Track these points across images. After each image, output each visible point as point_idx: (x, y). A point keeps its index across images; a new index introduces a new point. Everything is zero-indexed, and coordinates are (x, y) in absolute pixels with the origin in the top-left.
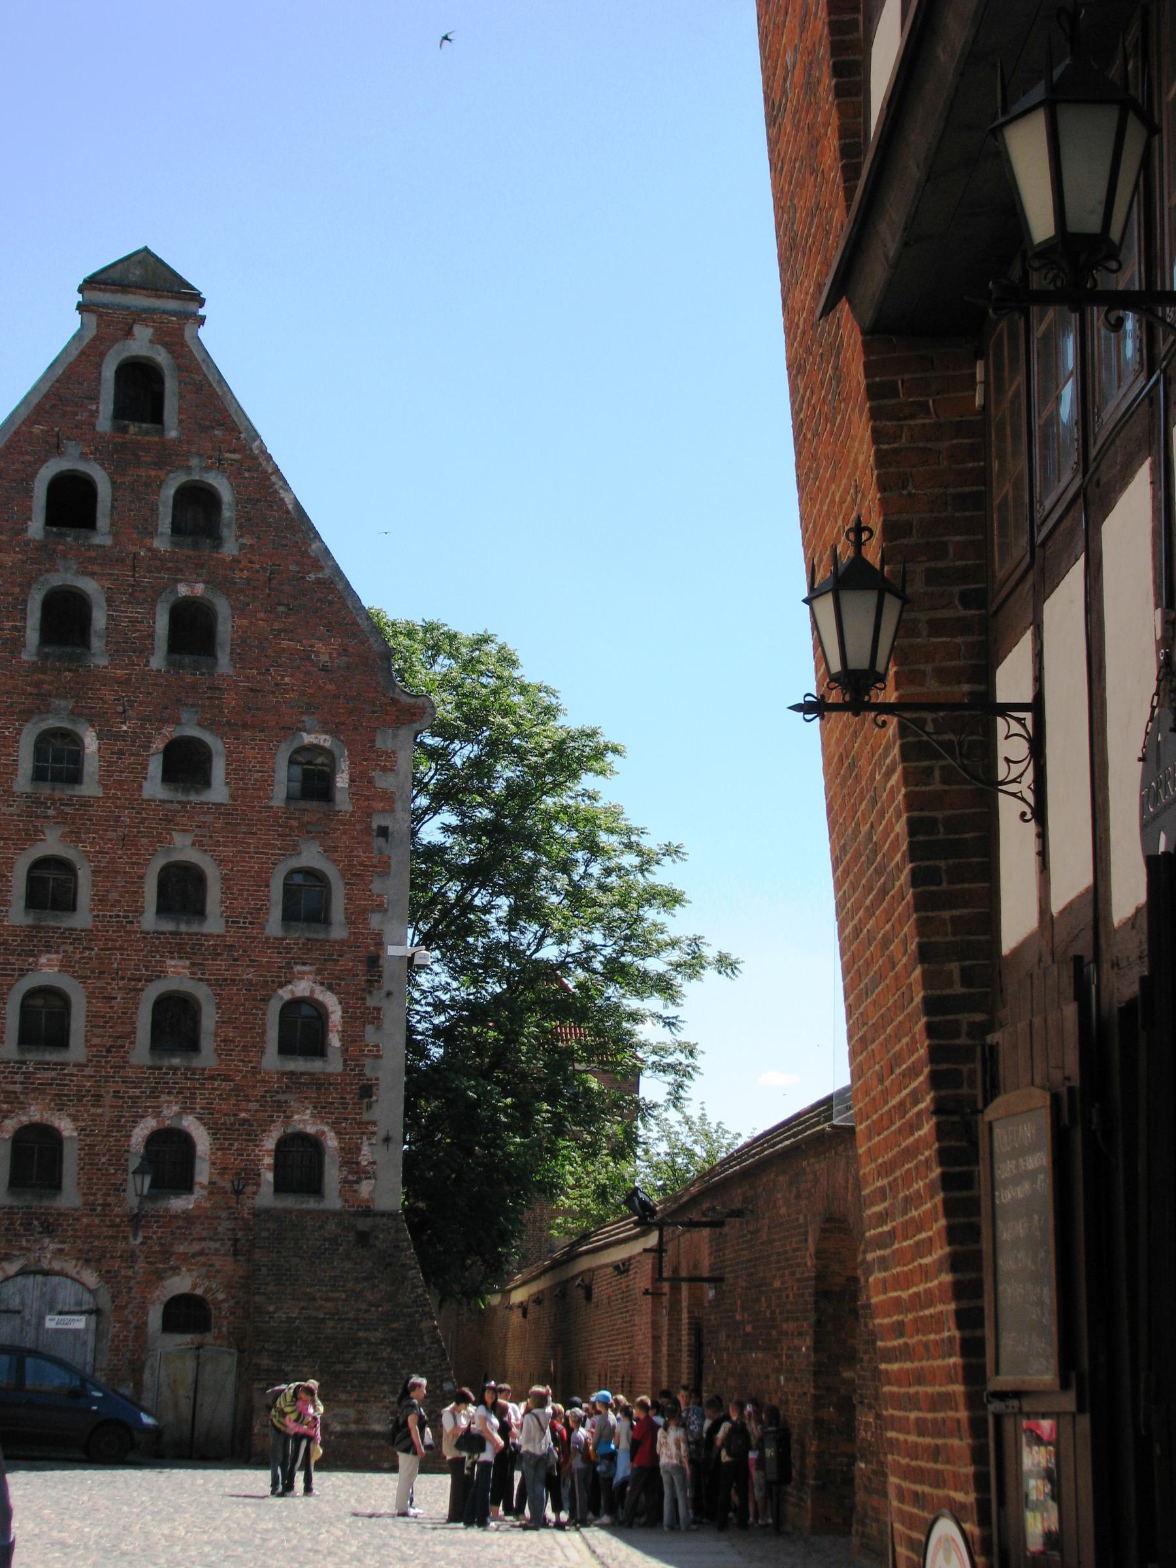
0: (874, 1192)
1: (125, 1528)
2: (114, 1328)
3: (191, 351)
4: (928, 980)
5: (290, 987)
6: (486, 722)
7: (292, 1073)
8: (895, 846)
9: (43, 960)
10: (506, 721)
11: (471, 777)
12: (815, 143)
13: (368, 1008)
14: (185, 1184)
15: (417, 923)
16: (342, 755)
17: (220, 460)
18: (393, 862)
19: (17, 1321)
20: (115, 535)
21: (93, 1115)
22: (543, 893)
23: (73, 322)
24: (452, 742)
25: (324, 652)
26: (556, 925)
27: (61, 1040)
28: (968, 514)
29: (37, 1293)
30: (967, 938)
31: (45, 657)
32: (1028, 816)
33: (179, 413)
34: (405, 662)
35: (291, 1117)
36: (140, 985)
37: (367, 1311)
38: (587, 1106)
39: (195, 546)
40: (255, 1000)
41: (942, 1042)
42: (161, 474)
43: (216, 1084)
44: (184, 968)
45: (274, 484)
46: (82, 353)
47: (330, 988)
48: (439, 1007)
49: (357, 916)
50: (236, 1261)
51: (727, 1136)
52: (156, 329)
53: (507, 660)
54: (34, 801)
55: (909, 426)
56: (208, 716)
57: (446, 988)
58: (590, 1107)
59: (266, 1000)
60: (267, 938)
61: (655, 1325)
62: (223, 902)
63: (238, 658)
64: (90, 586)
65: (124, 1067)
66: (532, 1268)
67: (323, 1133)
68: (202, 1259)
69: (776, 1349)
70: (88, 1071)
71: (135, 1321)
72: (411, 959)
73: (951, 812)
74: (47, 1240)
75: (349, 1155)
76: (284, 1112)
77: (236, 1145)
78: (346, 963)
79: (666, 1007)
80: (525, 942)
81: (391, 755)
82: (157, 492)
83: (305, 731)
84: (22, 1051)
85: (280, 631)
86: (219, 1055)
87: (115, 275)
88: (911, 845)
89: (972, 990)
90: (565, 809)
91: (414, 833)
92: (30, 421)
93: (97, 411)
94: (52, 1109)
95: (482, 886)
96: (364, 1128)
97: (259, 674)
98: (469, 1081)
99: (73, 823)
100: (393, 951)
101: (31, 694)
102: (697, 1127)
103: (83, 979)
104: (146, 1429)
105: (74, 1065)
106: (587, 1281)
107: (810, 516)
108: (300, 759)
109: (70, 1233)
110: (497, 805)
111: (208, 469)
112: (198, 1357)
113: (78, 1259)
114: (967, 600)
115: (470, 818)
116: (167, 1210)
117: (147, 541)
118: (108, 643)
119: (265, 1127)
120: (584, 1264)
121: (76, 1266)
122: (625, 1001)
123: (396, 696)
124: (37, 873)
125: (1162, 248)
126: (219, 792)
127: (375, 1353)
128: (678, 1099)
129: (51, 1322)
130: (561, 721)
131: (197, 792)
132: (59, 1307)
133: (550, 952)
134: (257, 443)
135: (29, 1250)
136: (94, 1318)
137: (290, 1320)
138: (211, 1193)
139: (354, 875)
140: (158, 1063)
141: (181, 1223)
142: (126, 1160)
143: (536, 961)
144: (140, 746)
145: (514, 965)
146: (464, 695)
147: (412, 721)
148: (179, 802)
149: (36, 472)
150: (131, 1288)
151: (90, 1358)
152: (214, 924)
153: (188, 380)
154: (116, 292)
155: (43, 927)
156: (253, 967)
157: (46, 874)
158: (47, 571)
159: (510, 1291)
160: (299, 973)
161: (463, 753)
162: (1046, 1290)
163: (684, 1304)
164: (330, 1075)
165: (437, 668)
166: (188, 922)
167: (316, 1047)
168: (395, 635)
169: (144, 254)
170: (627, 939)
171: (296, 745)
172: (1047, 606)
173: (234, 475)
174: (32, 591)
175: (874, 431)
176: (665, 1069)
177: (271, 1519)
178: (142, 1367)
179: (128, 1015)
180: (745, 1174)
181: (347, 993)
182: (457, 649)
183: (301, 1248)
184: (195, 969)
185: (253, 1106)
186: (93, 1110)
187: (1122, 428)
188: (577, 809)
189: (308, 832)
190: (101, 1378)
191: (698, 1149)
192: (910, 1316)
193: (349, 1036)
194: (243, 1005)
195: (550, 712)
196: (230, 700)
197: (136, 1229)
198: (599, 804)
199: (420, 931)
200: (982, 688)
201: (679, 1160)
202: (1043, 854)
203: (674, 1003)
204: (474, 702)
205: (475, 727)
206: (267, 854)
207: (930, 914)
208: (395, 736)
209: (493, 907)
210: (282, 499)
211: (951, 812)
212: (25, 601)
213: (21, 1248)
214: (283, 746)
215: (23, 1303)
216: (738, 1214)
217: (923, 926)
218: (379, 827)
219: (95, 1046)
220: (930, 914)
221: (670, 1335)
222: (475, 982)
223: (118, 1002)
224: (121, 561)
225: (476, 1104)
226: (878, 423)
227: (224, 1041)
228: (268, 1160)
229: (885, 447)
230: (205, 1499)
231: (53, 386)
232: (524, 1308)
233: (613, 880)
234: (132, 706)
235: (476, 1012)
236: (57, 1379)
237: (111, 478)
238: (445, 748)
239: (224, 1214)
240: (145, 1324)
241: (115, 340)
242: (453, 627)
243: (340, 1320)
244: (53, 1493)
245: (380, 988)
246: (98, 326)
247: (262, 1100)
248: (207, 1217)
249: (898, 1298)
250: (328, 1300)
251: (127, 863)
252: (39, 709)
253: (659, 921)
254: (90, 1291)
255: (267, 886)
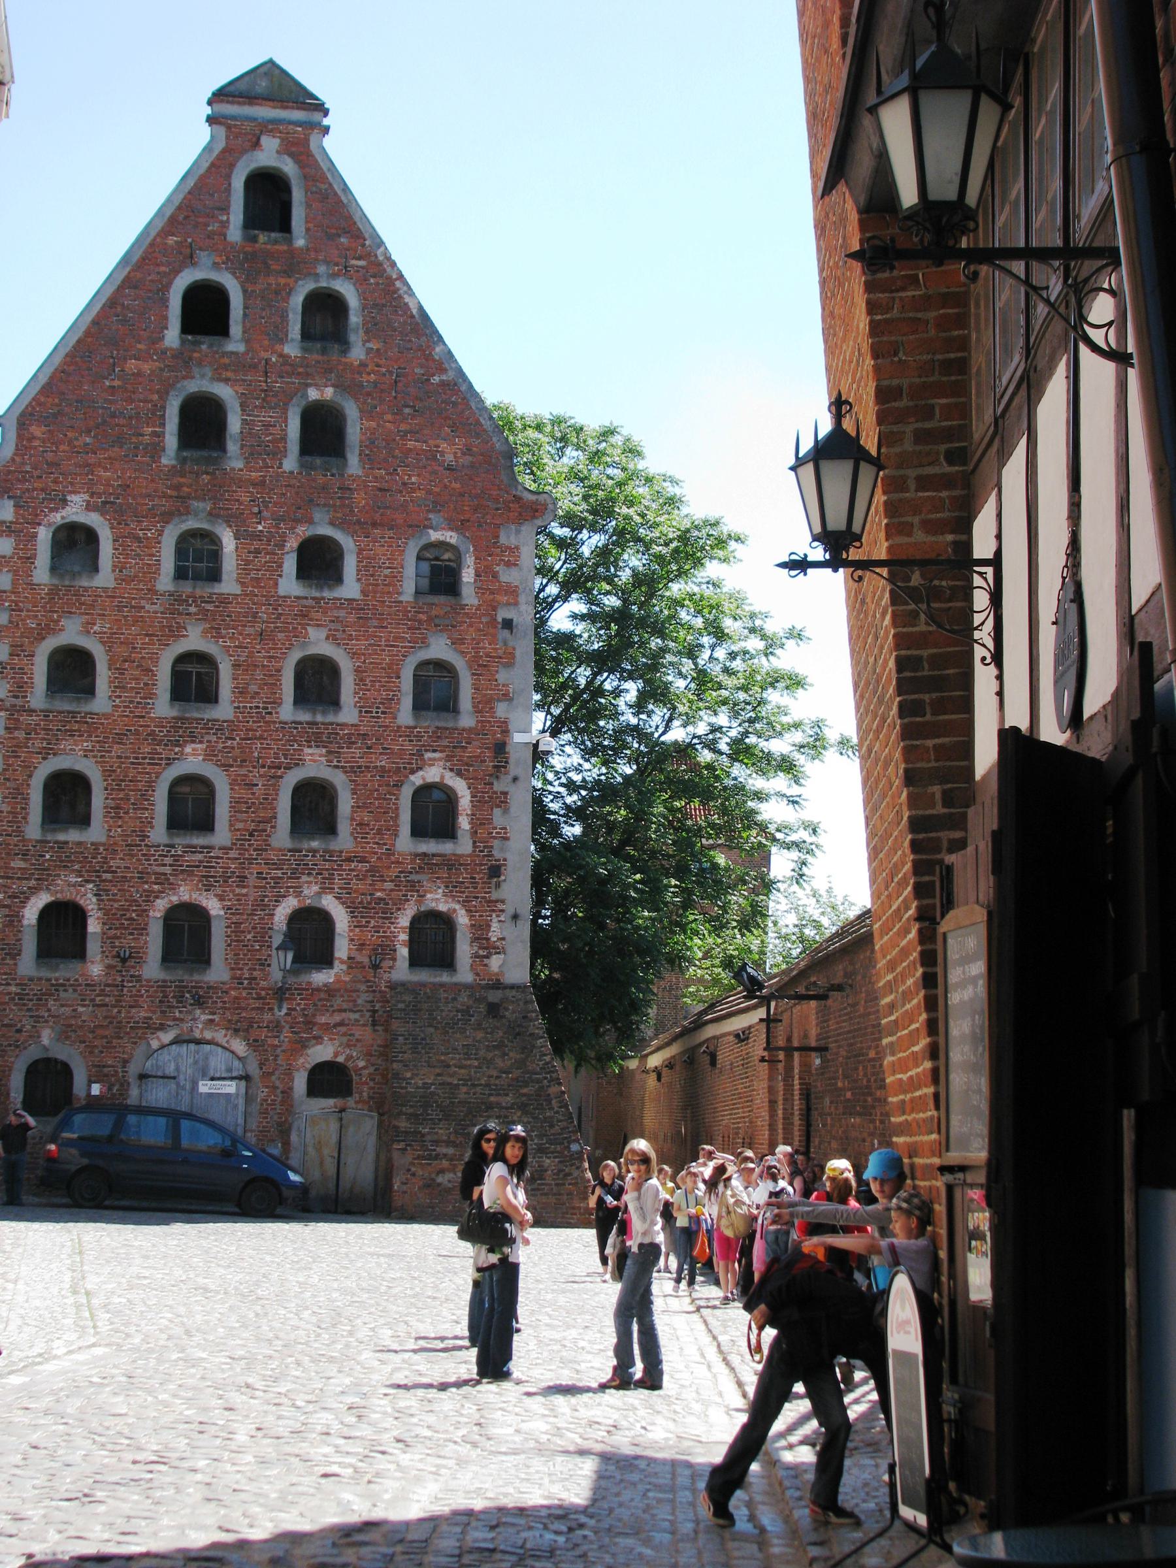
0: (885, 985)
1: (264, 1276)
2: (262, 1093)
3: (317, 161)
4: (913, 801)
5: (421, 773)
6: (610, 514)
7: (425, 854)
8: (889, 680)
9: (188, 749)
10: (631, 511)
11: (597, 565)
12: (827, 24)
13: (496, 793)
14: (325, 959)
15: (549, 708)
16: (468, 551)
17: (346, 267)
18: (518, 653)
19: (172, 1085)
20: (247, 341)
21: (238, 895)
22: (670, 678)
23: (204, 134)
24: (580, 533)
25: (449, 452)
26: (681, 709)
27: (206, 824)
28: (953, 378)
29: (191, 1061)
30: (948, 764)
31: (183, 461)
32: (988, 660)
33: (307, 222)
34: (533, 455)
35: (424, 896)
36: (279, 773)
37: (498, 1077)
38: (713, 881)
39: (324, 351)
40: (388, 785)
41: (924, 857)
42: (291, 281)
43: (353, 865)
44: (321, 756)
45: (398, 289)
46: (213, 165)
47: (459, 774)
48: (571, 787)
49: (484, 705)
50: (375, 1031)
51: (853, 908)
52: (282, 140)
53: (633, 451)
54: (177, 599)
55: (901, 298)
56: (339, 515)
57: (578, 769)
58: (718, 882)
59: (398, 785)
60: (399, 727)
61: (771, 1090)
62: (356, 693)
63: (367, 458)
64: (225, 392)
65: (266, 850)
66: (667, 1035)
67: (455, 910)
68: (343, 1029)
69: (871, 1115)
70: (233, 854)
71: (281, 1086)
72: (536, 746)
73: (935, 651)
74: (198, 1012)
75: (480, 933)
76: (418, 891)
77: (373, 923)
78: (473, 750)
79: (790, 786)
80: (653, 724)
81: (514, 550)
82: (286, 300)
83: (431, 528)
84: (170, 835)
85: (406, 432)
86: (356, 838)
87: (242, 86)
88: (900, 681)
89: (952, 810)
90: (691, 596)
91: (543, 622)
92: (165, 232)
93: (228, 221)
94: (200, 890)
95: (611, 671)
96: (493, 905)
97: (387, 474)
98: (599, 857)
99: (214, 620)
100: (518, 738)
101: (171, 497)
102: (824, 899)
103: (226, 767)
104: (293, 1185)
105: (220, 849)
106: (712, 1048)
107: (831, 366)
108: (428, 555)
109: (220, 1005)
110: (624, 594)
111: (334, 276)
112: (341, 1119)
113: (227, 1029)
114: (951, 457)
115: (598, 605)
116: (309, 983)
117: (278, 347)
118: (242, 448)
119: (400, 904)
120: (710, 1031)
121: (226, 1036)
122: (750, 781)
123: (518, 493)
124: (181, 667)
125: (1074, 169)
126: (350, 588)
127: (506, 1117)
128: (801, 876)
129: (205, 1087)
130: (685, 510)
131: (331, 588)
132: (212, 1073)
133: (677, 734)
134: (382, 249)
135: (182, 1020)
136: (243, 1083)
137: (426, 1086)
138: (350, 967)
139: (479, 665)
140: (298, 846)
141: (322, 995)
142: (270, 937)
143: (663, 743)
144: (275, 545)
145: (642, 748)
146: (589, 487)
147: (534, 517)
148: (313, 598)
149: (170, 283)
150: (277, 1056)
151: (241, 1121)
152: (348, 714)
153: (314, 189)
154: (244, 104)
155: (187, 719)
156: (386, 754)
157: (189, 668)
158: (185, 378)
159: (647, 1055)
160: (430, 759)
161: (590, 543)
162: (983, 1080)
163: (796, 1071)
164: (461, 856)
165: (565, 460)
166: (324, 713)
167: (447, 831)
168: (525, 428)
169: (269, 65)
170: (751, 721)
171: (423, 541)
172: (1005, 471)
173: (360, 281)
174: (170, 398)
175: (868, 303)
176: (788, 846)
177: (400, 1268)
178: (289, 1129)
179: (269, 801)
180: (844, 951)
181: (476, 779)
182: (585, 441)
183: (435, 1019)
184: (331, 757)
185: (389, 885)
186: (238, 891)
187: (1047, 327)
188: (702, 596)
189: (436, 626)
190: (251, 1138)
191: (825, 921)
192: (909, 1096)
193: (478, 819)
194: (377, 790)
195: (672, 502)
196: (360, 499)
197: (281, 1001)
198: (725, 590)
199: (551, 714)
200: (964, 537)
201: (807, 931)
202: (1000, 694)
203: (797, 782)
204: (600, 493)
205: (602, 517)
206: (397, 646)
207: (915, 743)
208: (518, 532)
209: (621, 691)
210: (406, 304)
211: (935, 651)
212: (164, 408)
213: (175, 1019)
214: (411, 543)
215: (177, 1069)
216: (839, 988)
217: (908, 753)
218: (504, 620)
219: (238, 830)
220: (915, 743)
221: (785, 1100)
222: (605, 763)
223: (259, 790)
224: (254, 367)
225: (603, 881)
226: (871, 296)
227: (360, 824)
228: (404, 937)
229: (879, 317)
230: (343, 1250)
231: (185, 198)
232: (658, 1072)
233: (737, 664)
234: (266, 507)
235: (605, 792)
236: (209, 1140)
237: (242, 287)
238: (572, 539)
239: (363, 987)
240: (291, 1089)
241: (243, 152)
242: (580, 419)
243: (474, 1085)
244: (204, 1243)
245: (506, 773)
246: (227, 138)
247: (396, 880)
248: (346, 990)
249: (901, 1080)
250: (461, 1067)
251: (264, 657)
252: (179, 511)
253: (782, 704)
254: (239, 1058)
255: (399, 677)
